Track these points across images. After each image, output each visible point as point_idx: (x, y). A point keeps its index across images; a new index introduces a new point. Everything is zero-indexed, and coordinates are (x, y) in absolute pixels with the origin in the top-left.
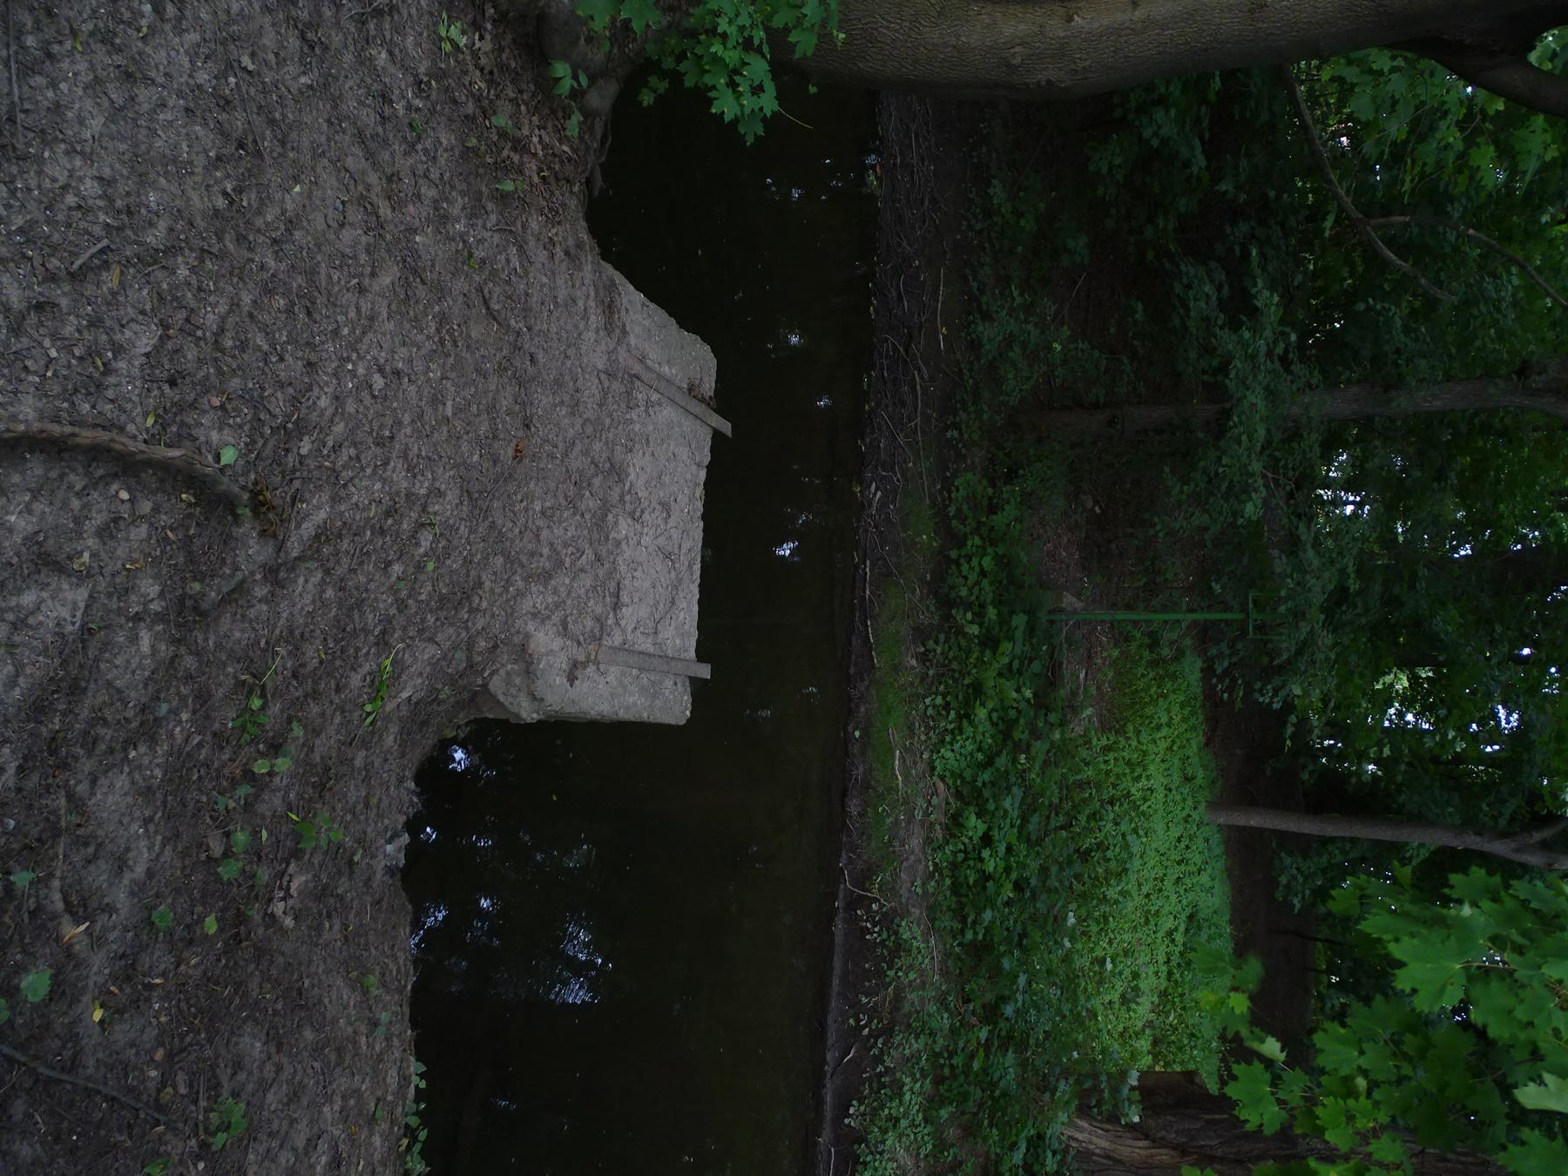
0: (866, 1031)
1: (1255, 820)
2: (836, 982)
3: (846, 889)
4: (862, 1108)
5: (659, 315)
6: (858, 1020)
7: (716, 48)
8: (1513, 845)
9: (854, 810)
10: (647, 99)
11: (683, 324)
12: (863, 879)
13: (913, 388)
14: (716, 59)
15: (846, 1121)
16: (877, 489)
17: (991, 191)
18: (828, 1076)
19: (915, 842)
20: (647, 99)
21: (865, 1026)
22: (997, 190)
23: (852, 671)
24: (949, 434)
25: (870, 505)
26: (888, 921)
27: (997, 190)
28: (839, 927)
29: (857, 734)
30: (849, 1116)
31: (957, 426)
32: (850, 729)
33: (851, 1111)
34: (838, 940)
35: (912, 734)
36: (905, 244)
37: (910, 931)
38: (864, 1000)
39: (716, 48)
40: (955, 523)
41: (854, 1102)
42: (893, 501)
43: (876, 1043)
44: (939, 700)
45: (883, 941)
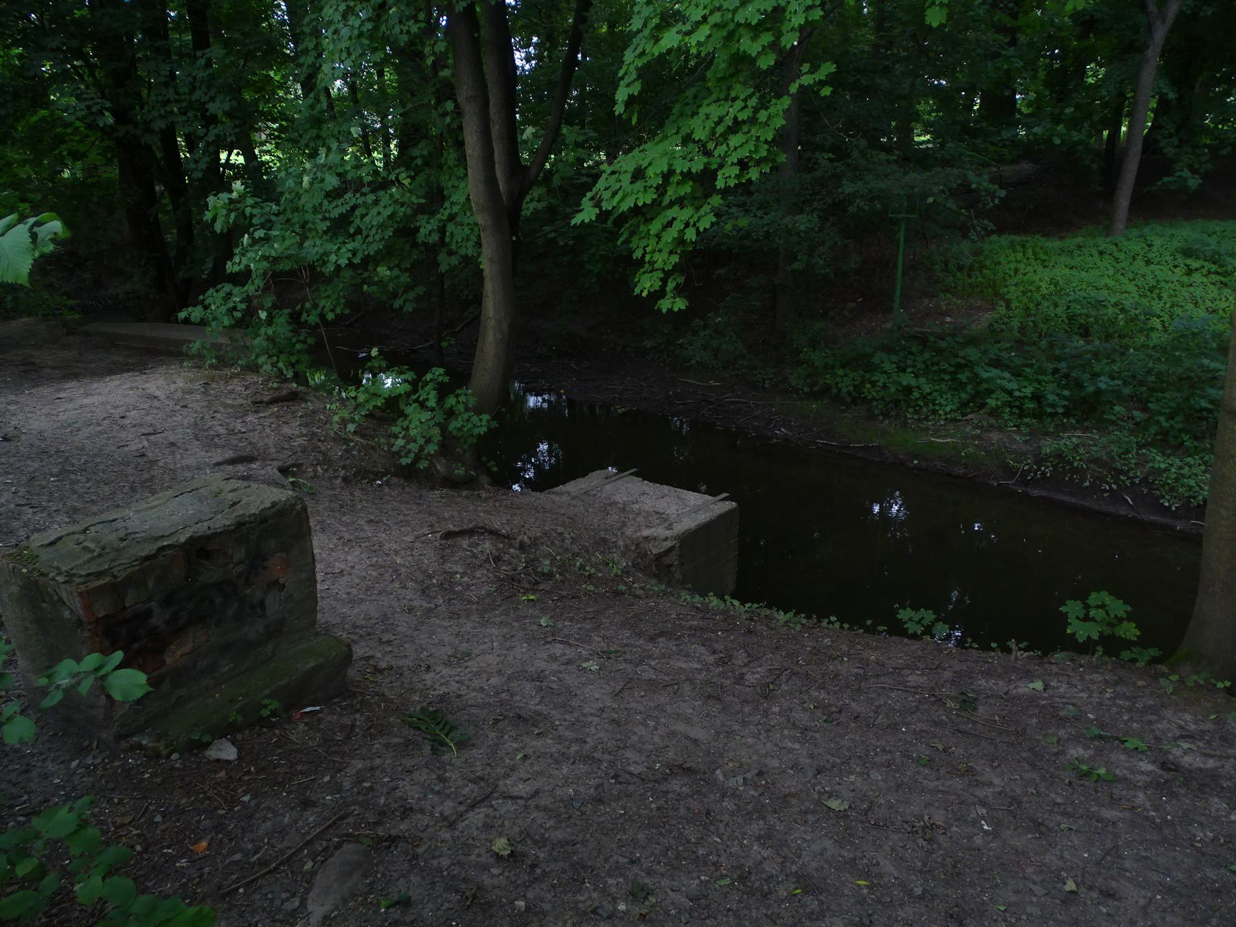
0: (1114, 486)
1: (1123, 201)
2: (1073, 500)
3: (1014, 484)
4: (1167, 497)
5: (572, 483)
6: (1105, 491)
7: (465, 429)
8: (1158, 23)
9: (962, 471)
10: (495, 469)
11: (584, 476)
12: (1009, 472)
13: (733, 403)
14: (469, 430)
15: (1174, 509)
16: (779, 430)
17: (648, 346)
18: (1136, 515)
19: (995, 436)
20: (495, 469)
21: (1110, 486)
22: (648, 344)
23: (877, 459)
24: (767, 386)
25: (787, 435)
26: (1040, 460)
27: (648, 344)
28: (1035, 493)
29: (916, 462)
30: (1170, 507)
31: (764, 380)
32: (910, 465)
33: (1167, 504)
34: (1044, 493)
35: (927, 429)
36: (658, 398)
37: (1048, 446)
38: (1087, 484)
39: (465, 429)
40: (815, 389)
41: (1161, 501)
42: (790, 421)
43: (1122, 481)
44: (911, 410)
45: (1052, 466)
